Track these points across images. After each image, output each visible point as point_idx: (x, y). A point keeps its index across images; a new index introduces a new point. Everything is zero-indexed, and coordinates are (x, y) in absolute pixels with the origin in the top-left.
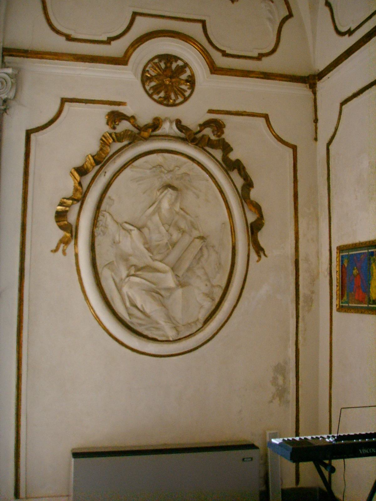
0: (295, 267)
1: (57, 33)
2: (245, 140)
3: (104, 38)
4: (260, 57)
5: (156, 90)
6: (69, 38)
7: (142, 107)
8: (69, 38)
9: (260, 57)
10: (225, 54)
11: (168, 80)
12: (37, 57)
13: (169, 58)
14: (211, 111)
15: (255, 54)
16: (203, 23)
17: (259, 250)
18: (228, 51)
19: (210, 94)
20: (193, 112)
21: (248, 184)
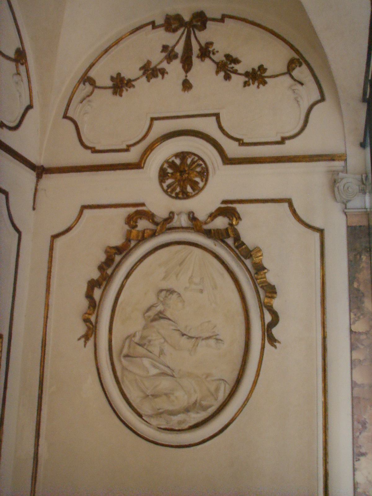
0: (44, 384)
1: (138, 144)
2: (254, 227)
3: (124, 147)
4: (283, 141)
5: (194, 185)
6: (94, 151)
7: (160, 203)
8: (94, 151)
9: (283, 141)
10: (241, 142)
11: (183, 176)
12: (92, 170)
13: (183, 155)
14: (224, 202)
15: (279, 139)
16: (217, 116)
17: (273, 340)
18: (98, 148)
19: (222, 184)
20: (204, 203)
21: (92, 285)
